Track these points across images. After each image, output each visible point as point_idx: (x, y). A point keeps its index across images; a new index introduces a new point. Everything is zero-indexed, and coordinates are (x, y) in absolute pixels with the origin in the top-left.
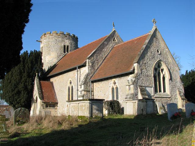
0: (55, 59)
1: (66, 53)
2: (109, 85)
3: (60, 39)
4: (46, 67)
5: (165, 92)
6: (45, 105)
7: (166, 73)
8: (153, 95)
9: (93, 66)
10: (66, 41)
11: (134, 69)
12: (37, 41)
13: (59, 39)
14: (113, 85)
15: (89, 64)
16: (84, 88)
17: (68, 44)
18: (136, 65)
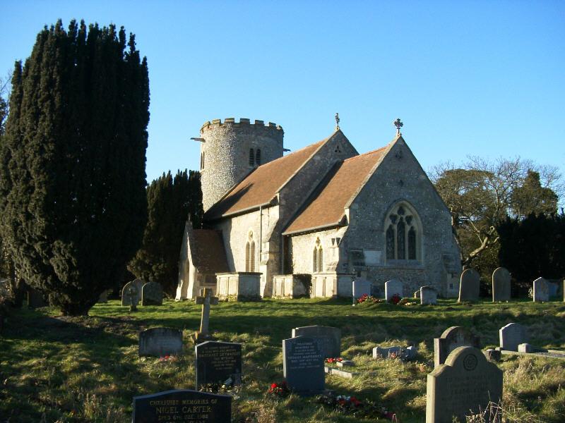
12: (192, 139)
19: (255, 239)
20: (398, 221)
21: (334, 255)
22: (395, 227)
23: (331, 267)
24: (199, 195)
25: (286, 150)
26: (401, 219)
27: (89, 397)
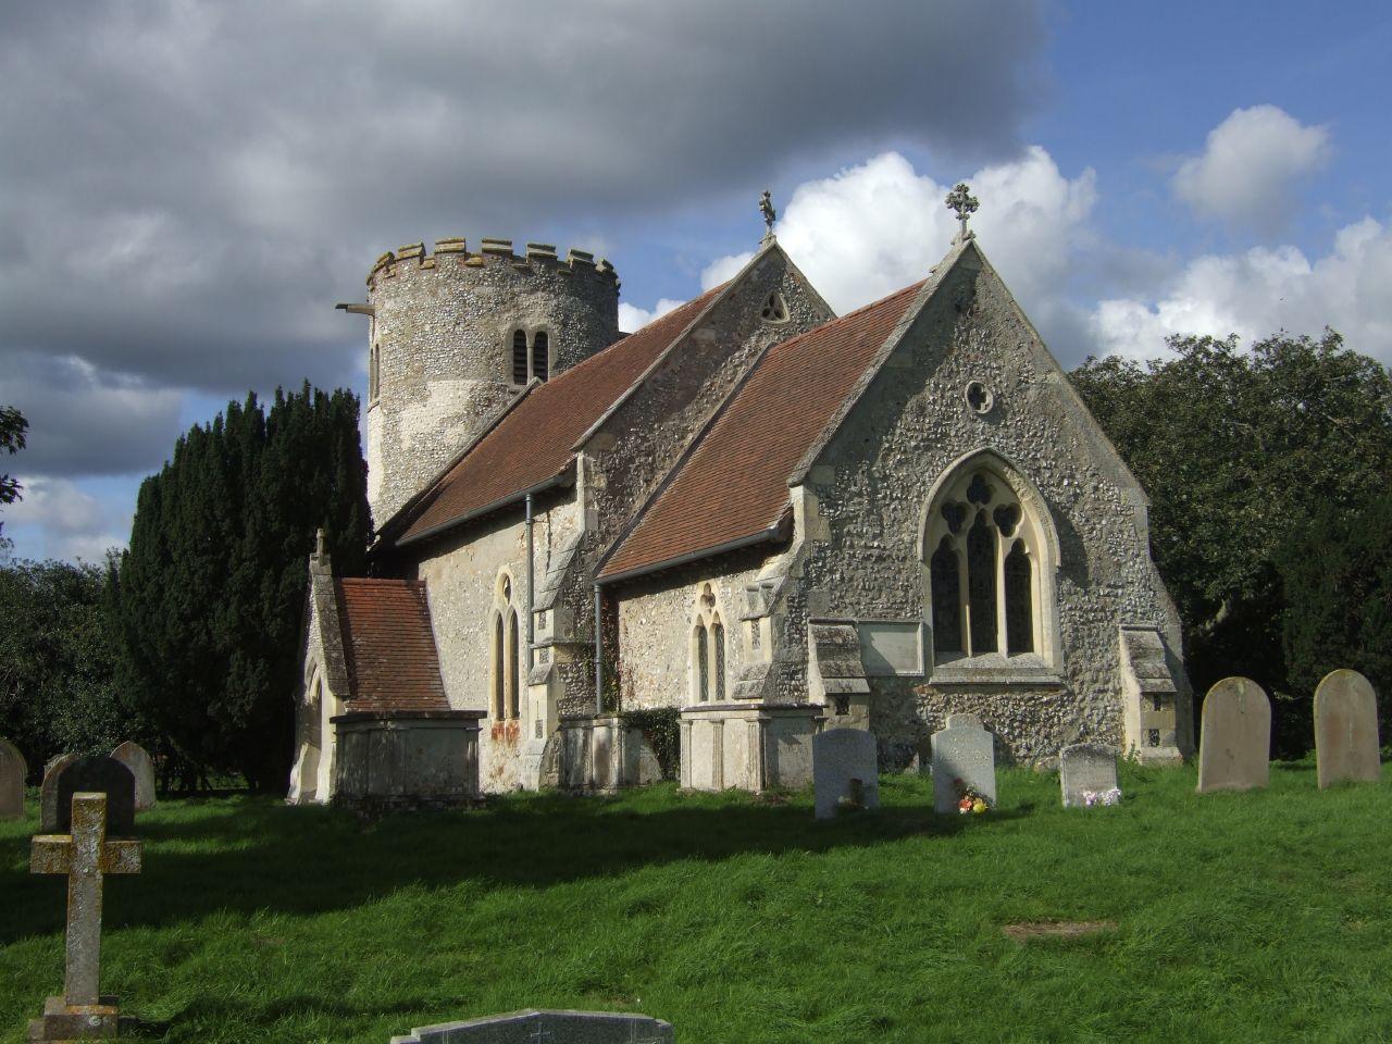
0: (460, 428)
1: (531, 380)
2: (687, 611)
3: (487, 290)
4: (384, 494)
5: (1031, 649)
6: (1147, 738)
7: (1038, 535)
8: (920, 670)
9: (617, 490)
10: (525, 300)
11: (788, 524)
12: (340, 307)
13: (477, 290)
14: (700, 608)
15: (587, 478)
16: (556, 629)
17: (544, 321)
18: (797, 495)
19: (518, 603)
20: (969, 523)
21: (756, 642)
22: (961, 545)
23: (748, 683)
24: (357, 470)
25: (549, 516)
26: (981, 516)
27: (955, 361)
